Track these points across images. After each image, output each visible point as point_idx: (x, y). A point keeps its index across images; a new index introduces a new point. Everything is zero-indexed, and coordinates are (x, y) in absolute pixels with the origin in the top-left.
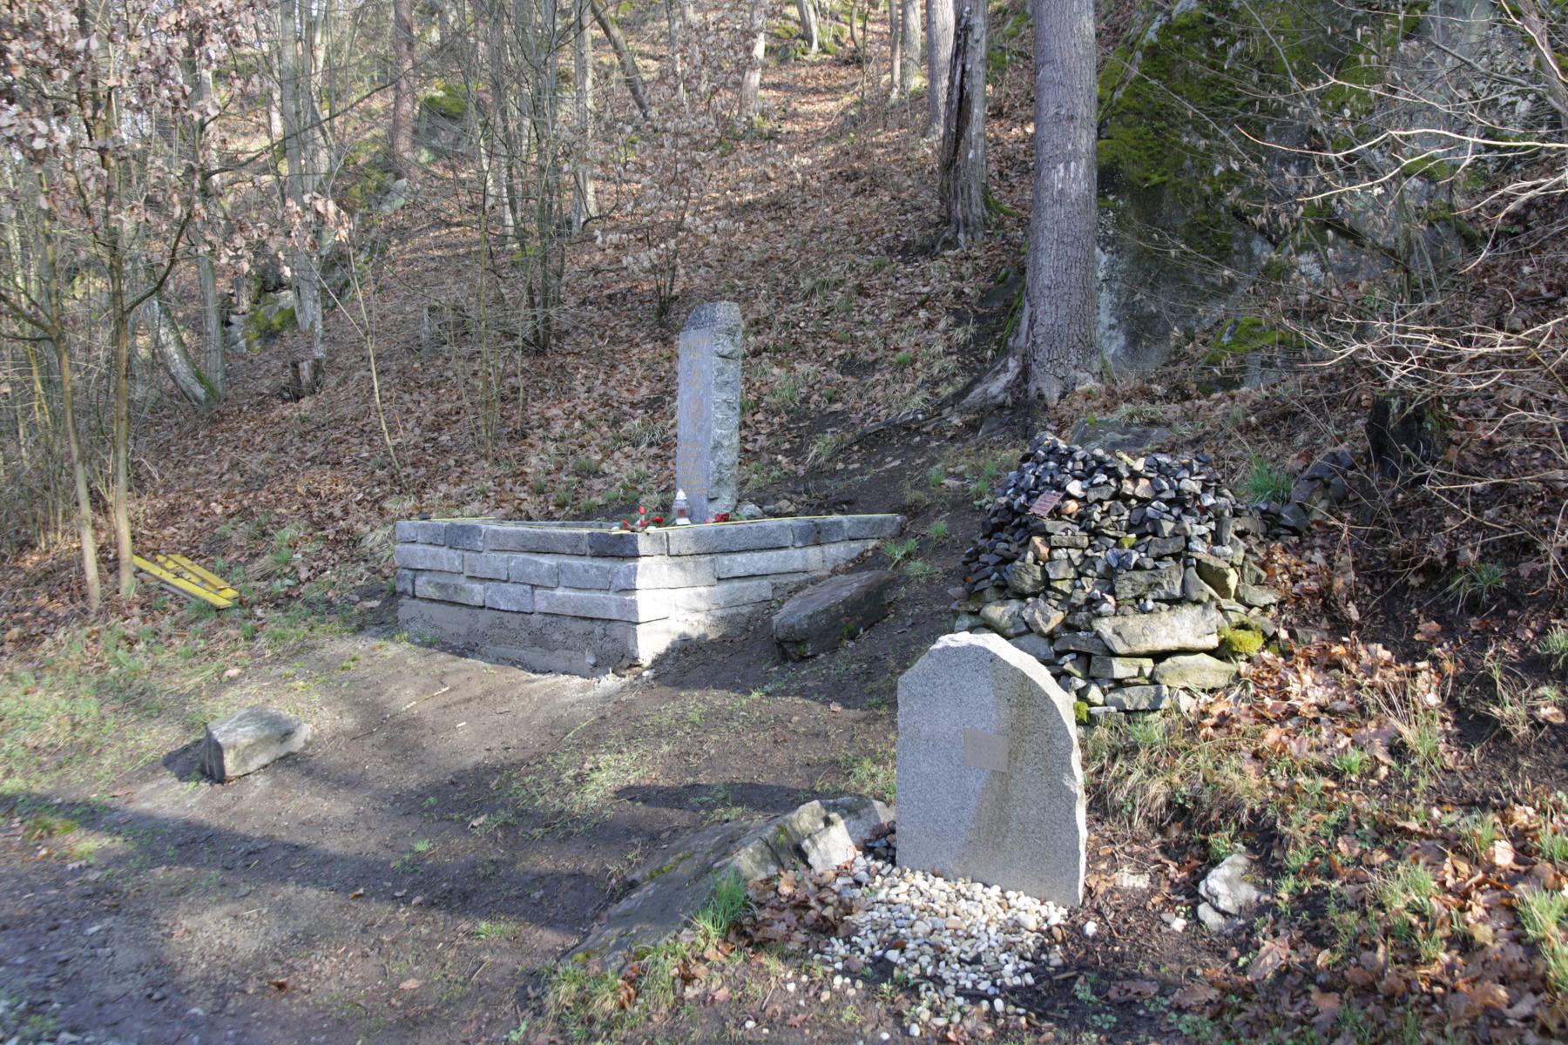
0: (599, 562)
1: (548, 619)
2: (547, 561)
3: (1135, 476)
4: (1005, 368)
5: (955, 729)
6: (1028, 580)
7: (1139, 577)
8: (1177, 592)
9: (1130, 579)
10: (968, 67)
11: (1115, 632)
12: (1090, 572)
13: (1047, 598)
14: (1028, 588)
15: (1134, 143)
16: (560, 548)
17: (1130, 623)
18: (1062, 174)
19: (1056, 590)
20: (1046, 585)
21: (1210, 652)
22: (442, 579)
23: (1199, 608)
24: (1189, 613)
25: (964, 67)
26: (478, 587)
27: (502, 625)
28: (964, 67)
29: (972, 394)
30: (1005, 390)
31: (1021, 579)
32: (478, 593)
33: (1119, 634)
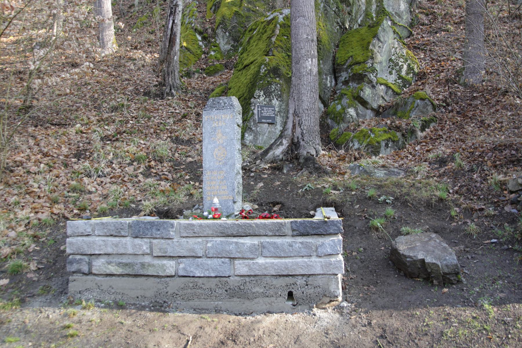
0: (300, 239)
1: (247, 279)
2: (248, 241)
4: (281, 144)
10: (176, 21)
15: (282, 59)
16: (262, 232)
18: (310, 62)
22: (125, 260)
25: (174, 21)
26: (172, 263)
27: (196, 286)
28: (174, 21)
29: (269, 154)
30: (282, 153)
32: (170, 267)
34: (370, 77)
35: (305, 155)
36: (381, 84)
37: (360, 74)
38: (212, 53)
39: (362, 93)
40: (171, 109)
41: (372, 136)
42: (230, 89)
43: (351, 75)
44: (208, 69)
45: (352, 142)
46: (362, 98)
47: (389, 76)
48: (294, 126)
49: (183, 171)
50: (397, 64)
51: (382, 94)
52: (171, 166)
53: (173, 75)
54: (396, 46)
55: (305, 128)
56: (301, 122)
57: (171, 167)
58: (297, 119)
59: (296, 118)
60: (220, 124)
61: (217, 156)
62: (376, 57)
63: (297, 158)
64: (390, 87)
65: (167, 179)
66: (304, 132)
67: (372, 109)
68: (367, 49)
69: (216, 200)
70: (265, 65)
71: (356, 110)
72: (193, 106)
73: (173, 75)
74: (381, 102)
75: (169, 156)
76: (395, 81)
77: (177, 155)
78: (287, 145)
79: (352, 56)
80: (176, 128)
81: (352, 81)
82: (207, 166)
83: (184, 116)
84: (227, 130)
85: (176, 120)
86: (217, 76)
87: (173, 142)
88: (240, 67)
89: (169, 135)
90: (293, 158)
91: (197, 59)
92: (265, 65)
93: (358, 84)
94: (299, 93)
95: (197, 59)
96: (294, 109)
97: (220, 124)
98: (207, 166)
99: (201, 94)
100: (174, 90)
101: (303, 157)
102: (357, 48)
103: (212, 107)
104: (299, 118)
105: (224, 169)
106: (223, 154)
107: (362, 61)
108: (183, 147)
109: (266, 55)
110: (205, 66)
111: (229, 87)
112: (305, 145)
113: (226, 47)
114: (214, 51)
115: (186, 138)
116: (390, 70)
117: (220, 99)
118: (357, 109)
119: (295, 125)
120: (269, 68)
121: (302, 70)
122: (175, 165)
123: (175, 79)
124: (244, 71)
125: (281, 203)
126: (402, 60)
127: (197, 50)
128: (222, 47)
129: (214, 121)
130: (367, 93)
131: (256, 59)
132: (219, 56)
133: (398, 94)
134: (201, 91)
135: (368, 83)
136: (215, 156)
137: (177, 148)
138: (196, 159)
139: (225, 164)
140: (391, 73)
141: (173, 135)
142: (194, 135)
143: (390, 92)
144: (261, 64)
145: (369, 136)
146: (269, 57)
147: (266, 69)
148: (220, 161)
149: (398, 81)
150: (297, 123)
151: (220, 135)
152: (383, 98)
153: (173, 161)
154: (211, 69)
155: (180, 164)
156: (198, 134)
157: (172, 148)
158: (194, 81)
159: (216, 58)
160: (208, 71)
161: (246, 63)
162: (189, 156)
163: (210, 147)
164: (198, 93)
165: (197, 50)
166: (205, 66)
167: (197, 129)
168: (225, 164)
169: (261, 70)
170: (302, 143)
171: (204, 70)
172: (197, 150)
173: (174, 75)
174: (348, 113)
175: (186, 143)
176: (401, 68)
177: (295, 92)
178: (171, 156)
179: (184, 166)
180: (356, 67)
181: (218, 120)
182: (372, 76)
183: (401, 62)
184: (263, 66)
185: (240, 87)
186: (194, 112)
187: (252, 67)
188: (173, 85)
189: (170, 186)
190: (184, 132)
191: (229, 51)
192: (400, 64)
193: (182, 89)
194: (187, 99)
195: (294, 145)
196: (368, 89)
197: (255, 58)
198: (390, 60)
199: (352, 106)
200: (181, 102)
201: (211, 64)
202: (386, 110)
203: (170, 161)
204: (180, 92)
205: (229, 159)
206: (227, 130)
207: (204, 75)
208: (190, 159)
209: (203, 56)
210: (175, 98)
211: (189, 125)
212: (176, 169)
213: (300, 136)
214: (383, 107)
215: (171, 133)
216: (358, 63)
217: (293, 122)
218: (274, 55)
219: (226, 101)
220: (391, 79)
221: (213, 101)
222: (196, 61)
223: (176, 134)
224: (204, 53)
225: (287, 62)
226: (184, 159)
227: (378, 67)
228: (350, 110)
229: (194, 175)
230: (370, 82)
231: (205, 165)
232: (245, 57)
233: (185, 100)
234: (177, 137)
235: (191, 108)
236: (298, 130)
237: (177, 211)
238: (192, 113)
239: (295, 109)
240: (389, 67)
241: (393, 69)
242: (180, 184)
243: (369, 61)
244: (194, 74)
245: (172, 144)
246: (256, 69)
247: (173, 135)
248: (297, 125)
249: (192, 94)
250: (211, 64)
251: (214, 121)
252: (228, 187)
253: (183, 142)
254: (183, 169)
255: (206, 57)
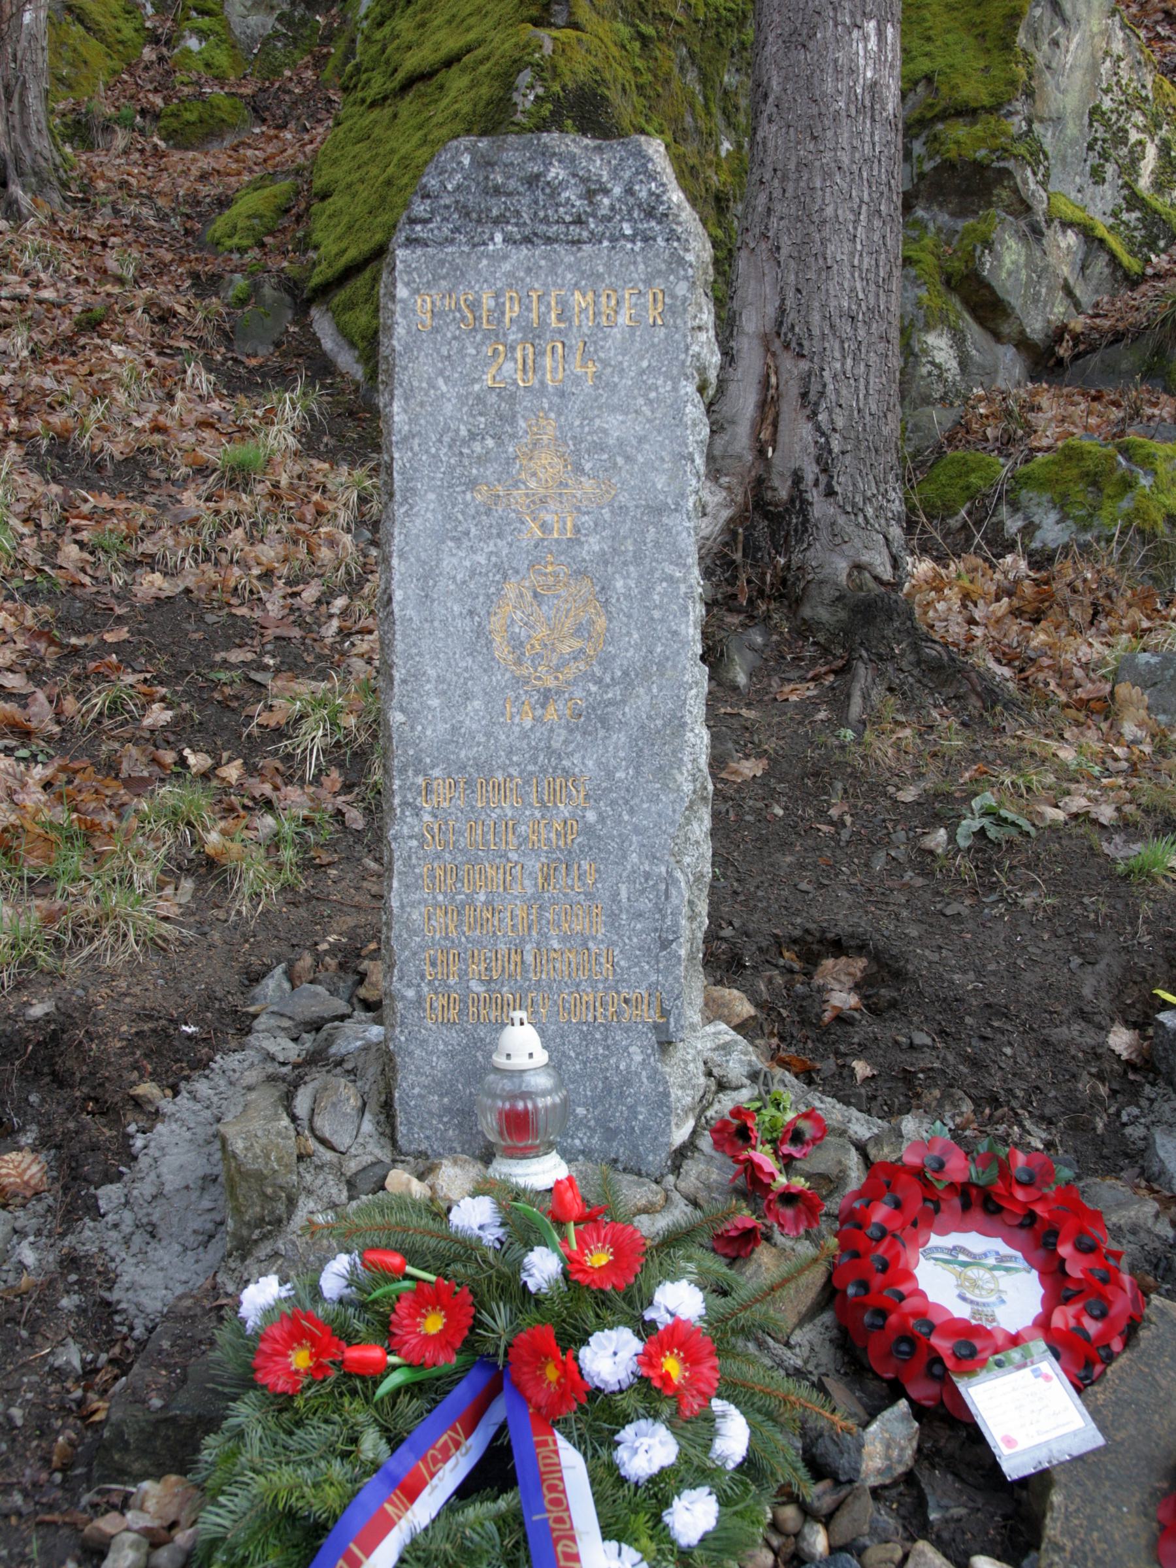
15: (615, 51)
18: (873, 44)
34: (1025, 182)
35: (843, 578)
36: (1066, 225)
37: (979, 167)
38: (193, 43)
39: (987, 258)
40: (13, 278)
41: (1145, 482)
42: (324, 196)
43: (928, 166)
44: (173, 115)
45: (1015, 507)
46: (989, 287)
47: (1090, 190)
48: (768, 404)
49: (127, 663)
50: (1120, 137)
51: (1065, 270)
52: (42, 633)
53: (15, 105)
54: (1118, 47)
55: (840, 423)
56: (815, 388)
57: (37, 635)
58: (791, 369)
59: (787, 362)
60: (552, 370)
61: (517, 645)
62: (1043, 85)
63: (788, 591)
64: (1102, 241)
65: (25, 734)
66: (836, 446)
67: (1023, 343)
68: (1006, 45)
69: (523, 1046)
70: (538, 68)
71: (958, 340)
72: (130, 273)
73: (15, 105)
74: (1059, 309)
75: (22, 563)
76: (1115, 215)
77: (71, 553)
78: (726, 514)
79: (929, 79)
80: (49, 383)
81: (931, 199)
82: (432, 731)
83: (91, 323)
84: (614, 425)
85: (47, 340)
86: (215, 148)
87: (40, 468)
88: (378, 84)
89: (14, 423)
90: (761, 593)
91: (117, 64)
92: (538, 68)
93: (961, 213)
94: (808, 217)
95: (117, 64)
96: (771, 310)
97: (552, 370)
98: (432, 731)
99: (162, 217)
100: (24, 187)
101: (829, 593)
102: (950, 38)
103: (473, 219)
104: (804, 365)
105: (586, 764)
106: (578, 631)
107: (987, 101)
108: (106, 502)
109: (537, 23)
110: (158, 101)
111: (318, 183)
112: (841, 520)
113: (253, 20)
114: (202, 34)
115: (116, 448)
116: (1093, 158)
117: (547, 155)
118: (964, 340)
119: (775, 401)
120: (556, 88)
121: (829, 87)
122: (64, 622)
123: (25, 127)
124: (406, 106)
125: (862, 949)
126: (1138, 118)
127: (120, 23)
128: (235, 19)
129: (496, 335)
130: (1008, 260)
131: (480, 43)
132: (222, 59)
133: (1134, 282)
134: (160, 202)
135: (1015, 214)
136: (501, 650)
137: (68, 506)
138: (190, 581)
139: (593, 720)
140: (1097, 176)
141: (36, 424)
142: (157, 429)
143: (1100, 265)
144: (517, 65)
145: (1127, 485)
146: (555, 33)
147: (540, 91)
148: (546, 697)
149: (1125, 216)
150: (792, 391)
151: (548, 465)
152: (1068, 291)
153: (51, 596)
154: (191, 116)
155: (98, 615)
156: (182, 425)
157: (35, 506)
158: (113, 161)
159: (208, 65)
160: (175, 124)
161: (412, 62)
162: (150, 562)
163: (454, 562)
164: (145, 211)
165: (120, 23)
166: (158, 101)
167: (171, 397)
168: (593, 720)
169: (516, 97)
170: (820, 508)
171: (157, 117)
172: (194, 522)
173: (23, 106)
174: (925, 352)
175: (118, 475)
176: (1135, 161)
177: (779, 208)
178: (34, 559)
179: (123, 633)
180: (958, 131)
181: (534, 334)
182: (1029, 181)
183: (1135, 126)
184: (526, 77)
185: (389, 183)
186: (139, 302)
187: (457, 81)
188: (18, 161)
189: (47, 785)
190: (99, 409)
191: (267, 41)
192: (1134, 136)
193: (65, 186)
194: (92, 235)
195: (767, 515)
196: (1012, 243)
197: (471, 36)
198: (1095, 111)
199: (944, 319)
200: (64, 246)
201: (186, 90)
202: (1092, 349)
203: (31, 594)
204: (56, 198)
205: (627, 680)
206: (614, 425)
207: (155, 139)
208: (152, 583)
209: (148, 54)
210: (30, 224)
211: (124, 372)
212: (76, 651)
213: (811, 471)
214: (1076, 338)
215: (23, 413)
216: (967, 112)
217: (765, 384)
218: (576, 26)
219: (599, 167)
220: (1100, 205)
221: (485, 163)
222: (114, 72)
223: (56, 419)
224: (154, 39)
225: (636, 71)
226: (118, 579)
227: (1047, 136)
228: (931, 339)
229: (201, 695)
230: (1024, 207)
231: (413, 717)
232: (409, 37)
233: (85, 239)
234: (61, 442)
235: (120, 280)
236: (797, 440)
237: (131, 1044)
238: (130, 310)
239: (782, 310)
240: (1090, 148)
241: (1104, 156)
242: (111, 767)
243: (1018, 105)
244: (107, 129)
245: (35, 477)
246: (484, 91)
247: (36, 424)
248: (789, 407)
249: (116, 212)
250: (186, 90)
251: (496, 335)
252: (613, 917)
253: (99, 468)
254: (117, 647)
255: (161, 59)
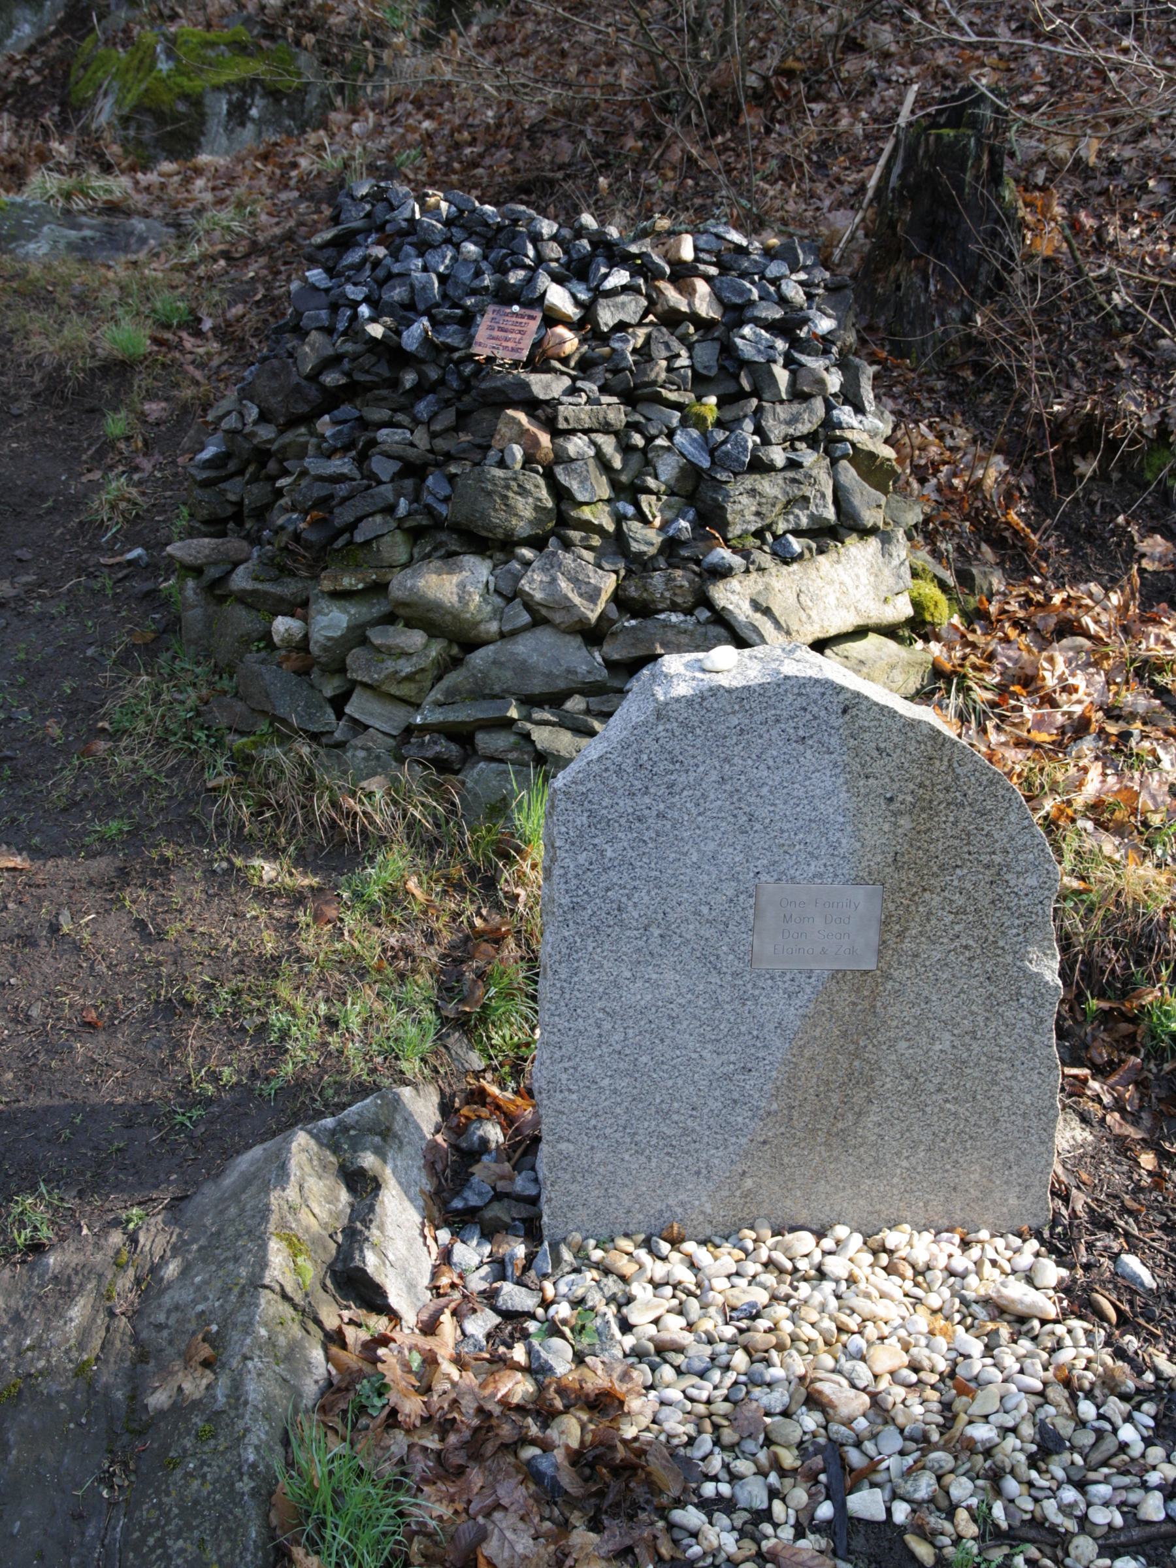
3: (682, 274)
5: (729, 890)
6: (525, 508)
7: (770, 487)
8: (830, 513)
9: (753, 492)
11: (756, 606)
12: (651, 482)
13: (567, 545)
14: (522, 528)
17: (776, 584)
19: (587, 527)
20: (560, 523)
21: (890, 631)
23: (874, 543)
24: (859, 554)
31: (510, 509)
33: (767, 611)
